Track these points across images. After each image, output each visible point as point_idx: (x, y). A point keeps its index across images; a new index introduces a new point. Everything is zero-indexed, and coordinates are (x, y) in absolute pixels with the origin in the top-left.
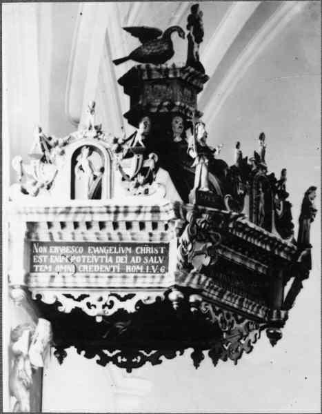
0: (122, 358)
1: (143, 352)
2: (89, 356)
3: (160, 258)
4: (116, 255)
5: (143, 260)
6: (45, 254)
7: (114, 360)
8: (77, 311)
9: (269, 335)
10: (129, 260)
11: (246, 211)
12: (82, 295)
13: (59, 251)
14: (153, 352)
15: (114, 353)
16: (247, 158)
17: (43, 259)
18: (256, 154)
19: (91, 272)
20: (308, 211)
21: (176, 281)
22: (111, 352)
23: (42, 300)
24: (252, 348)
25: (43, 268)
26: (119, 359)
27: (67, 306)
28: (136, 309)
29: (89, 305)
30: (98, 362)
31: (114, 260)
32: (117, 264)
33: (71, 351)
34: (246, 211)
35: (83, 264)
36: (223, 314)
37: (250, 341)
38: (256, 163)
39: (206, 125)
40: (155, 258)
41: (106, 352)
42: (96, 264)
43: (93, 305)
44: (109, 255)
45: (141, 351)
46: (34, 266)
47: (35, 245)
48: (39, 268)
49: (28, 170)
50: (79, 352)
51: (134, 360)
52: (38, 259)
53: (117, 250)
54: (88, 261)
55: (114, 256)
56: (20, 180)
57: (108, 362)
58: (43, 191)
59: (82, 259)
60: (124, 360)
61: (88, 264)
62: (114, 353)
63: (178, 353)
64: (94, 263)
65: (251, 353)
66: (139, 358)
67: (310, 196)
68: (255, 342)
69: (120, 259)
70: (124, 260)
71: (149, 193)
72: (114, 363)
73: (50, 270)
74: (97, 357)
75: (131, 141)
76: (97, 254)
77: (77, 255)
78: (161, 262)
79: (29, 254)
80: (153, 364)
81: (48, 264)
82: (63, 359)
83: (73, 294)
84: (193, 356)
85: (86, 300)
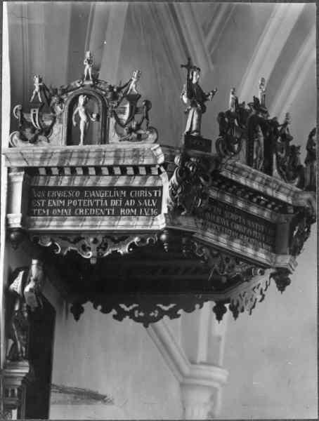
0: (139, 312)
1: (161, 306)
2: (106, 310)
3: (153, 201)
5: (137, 202)
6: (44, 198)
7: (131, 314)
9: (277, 282)
10: (124, 202)
11: (275, 171)
14: (172, 306)
15: (131, 308)
16: (244, 103)
17: (41, 203)
18: (256, 99)
19: (87, 215)
20: (311, 156)
21: (167, 224)
22: (128, 306)
24: (263, 296)
25: (41, 212)
26: (136, 314)
30: (115, 317)
31: (109, 203)
32: (112, 208)
33: (88, 306)
34: (275, 171)
36: (222, 258)
38: (254, 107)
40: (149, 201)
41: (123, 306)
44: (104, 199)
45: (158, 305)
50: (95, 307)
51: (152, 314)
55: (109, 200)
59: (78, 202)
60: (142, 314)
62: (131, 308)
63: (197, 306)
64: (90, 207)
65: (263, 302)
68: (266, 290)
69: (114, 203)
70: (119, 202)
74: (114, 312)
75: (126, 88)
76: (93, 198)
78: (154, 205)
80: (171, 318)
84: (215, 309)
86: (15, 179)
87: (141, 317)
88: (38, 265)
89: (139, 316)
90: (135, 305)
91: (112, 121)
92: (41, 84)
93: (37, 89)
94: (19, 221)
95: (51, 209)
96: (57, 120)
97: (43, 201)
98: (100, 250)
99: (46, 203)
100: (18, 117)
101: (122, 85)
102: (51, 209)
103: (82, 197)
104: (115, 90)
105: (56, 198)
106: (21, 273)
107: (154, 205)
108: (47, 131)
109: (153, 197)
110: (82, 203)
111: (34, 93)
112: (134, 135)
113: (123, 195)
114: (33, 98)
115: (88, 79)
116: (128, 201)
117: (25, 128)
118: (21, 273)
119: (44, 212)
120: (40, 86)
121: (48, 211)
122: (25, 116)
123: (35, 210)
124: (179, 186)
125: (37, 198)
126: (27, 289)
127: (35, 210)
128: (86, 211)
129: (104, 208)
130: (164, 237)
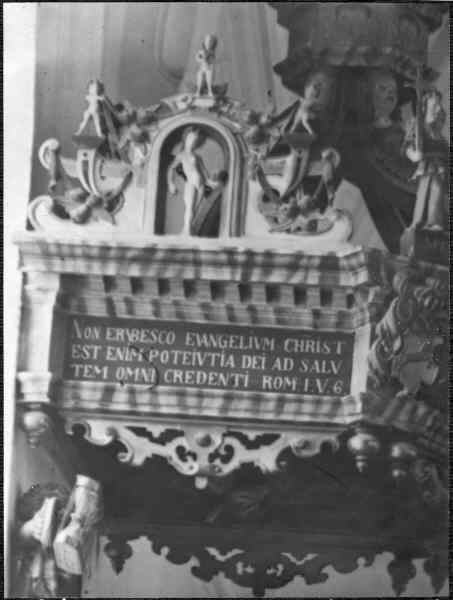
6: (96, 343)
15: (230, 555)
17: (91, 352)
25: (91, 371)
31: (238, 362)
32: (243, 372)
41: (213, 551)
50: (157, 550)
55: (238, 354)
59: (172, 357)
62: (230, 555)
64: (197, 367)
70: (259, 363)
74: (194, 562)
76: (203, 349)
84: (392, 567)
86: (34, 295)
87: (249, 574)
88: (89, 488)
89: (245, 572)
90: (236, 552)
91: (255, 188)
92: (101, 98)
93: (93, 109)
94: (45, 388)
95: (113, 366)
96: (135, 179)
97: (96, 348)
98: (217, 462)
99: (102, 353)
100: (48, 163)
101: (279, 112)
102: (113, 366)
103: (179, 344)
104: (264, 120)
105: (121, 345)
106: (49, 505)
107: (335, 371)
108: (112, 203)
109: (333, 356)
110: (180, 357)
111: (86, 116)
112: (302, 220)
113: (268, 347)
114: (83, 125)
115: (204, 91)
116: (278, 360)
117: (65, 189)
118: (49, 505)
119: (98, 371)
120: (99, 102)
121: (105, 369)
122: (64, 161)
123: (77, 367)
124: (396, 337)
125: (83, 342)
126: (61, 537)
127: (77, 367)
128: (188, 377)
129: (226, 370)
130: (356, 443)
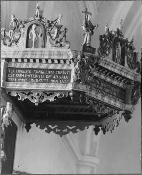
0: (58, 129)
1: (68, 127)
2: (42, 128)
3: (66, 76)
4: (46, 74)
5: (59, 77)
7: (54, 130)
8: (27, 100)
10: (52, 77)
12: (29, 93)
13: (20, 72)
14: (74, 127)
15: (54, 127)
16: (112, 31)
18: (118, 30)
23: (11, 94)
27: (22, 98)
28: (54, 100)
29: (32, 97)
30: (46, 131)
31: (45, 77)
33: (33, 125)
35: (31, 78)
37: (117, 121)
39: (92, 14)
40: (65, 76)
41: (50, 126)
42: (37, 78)
43: (34, 98)
44: (43, 74)
45: (67, 126)
46: (8, 78)
47: (9, 69)
48: (10, 80)
49: (8, 34)
50: (37, 126)
51: (64, 131)
52: (10, 75)
53: (47, 72)
54: (33, 77)
56: (4, 39)
57: (51, 131)
58: (14, 44)
59: (30, 76)
60: (59, 130)
61: (33, 78)
62: (54, 127)
63: (86, 128)
64: (36, 78)
66: (66, 129)
67: (68, 43)
68: (119, 121)
69: (48, 77)
71: (62, 46)
72: (54, 132)
73: (15, 81)
74: (46, 129)
76: (37, 74)
77: (29, 74)
79: (6, 73)
81: (15, 77)
82: (29, 130)
83: (25, 92)
84: (95, 129)
85: (31, 95)
